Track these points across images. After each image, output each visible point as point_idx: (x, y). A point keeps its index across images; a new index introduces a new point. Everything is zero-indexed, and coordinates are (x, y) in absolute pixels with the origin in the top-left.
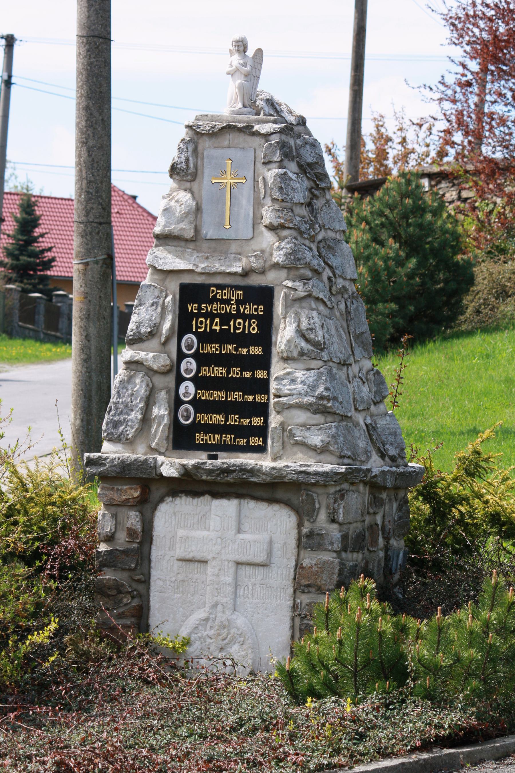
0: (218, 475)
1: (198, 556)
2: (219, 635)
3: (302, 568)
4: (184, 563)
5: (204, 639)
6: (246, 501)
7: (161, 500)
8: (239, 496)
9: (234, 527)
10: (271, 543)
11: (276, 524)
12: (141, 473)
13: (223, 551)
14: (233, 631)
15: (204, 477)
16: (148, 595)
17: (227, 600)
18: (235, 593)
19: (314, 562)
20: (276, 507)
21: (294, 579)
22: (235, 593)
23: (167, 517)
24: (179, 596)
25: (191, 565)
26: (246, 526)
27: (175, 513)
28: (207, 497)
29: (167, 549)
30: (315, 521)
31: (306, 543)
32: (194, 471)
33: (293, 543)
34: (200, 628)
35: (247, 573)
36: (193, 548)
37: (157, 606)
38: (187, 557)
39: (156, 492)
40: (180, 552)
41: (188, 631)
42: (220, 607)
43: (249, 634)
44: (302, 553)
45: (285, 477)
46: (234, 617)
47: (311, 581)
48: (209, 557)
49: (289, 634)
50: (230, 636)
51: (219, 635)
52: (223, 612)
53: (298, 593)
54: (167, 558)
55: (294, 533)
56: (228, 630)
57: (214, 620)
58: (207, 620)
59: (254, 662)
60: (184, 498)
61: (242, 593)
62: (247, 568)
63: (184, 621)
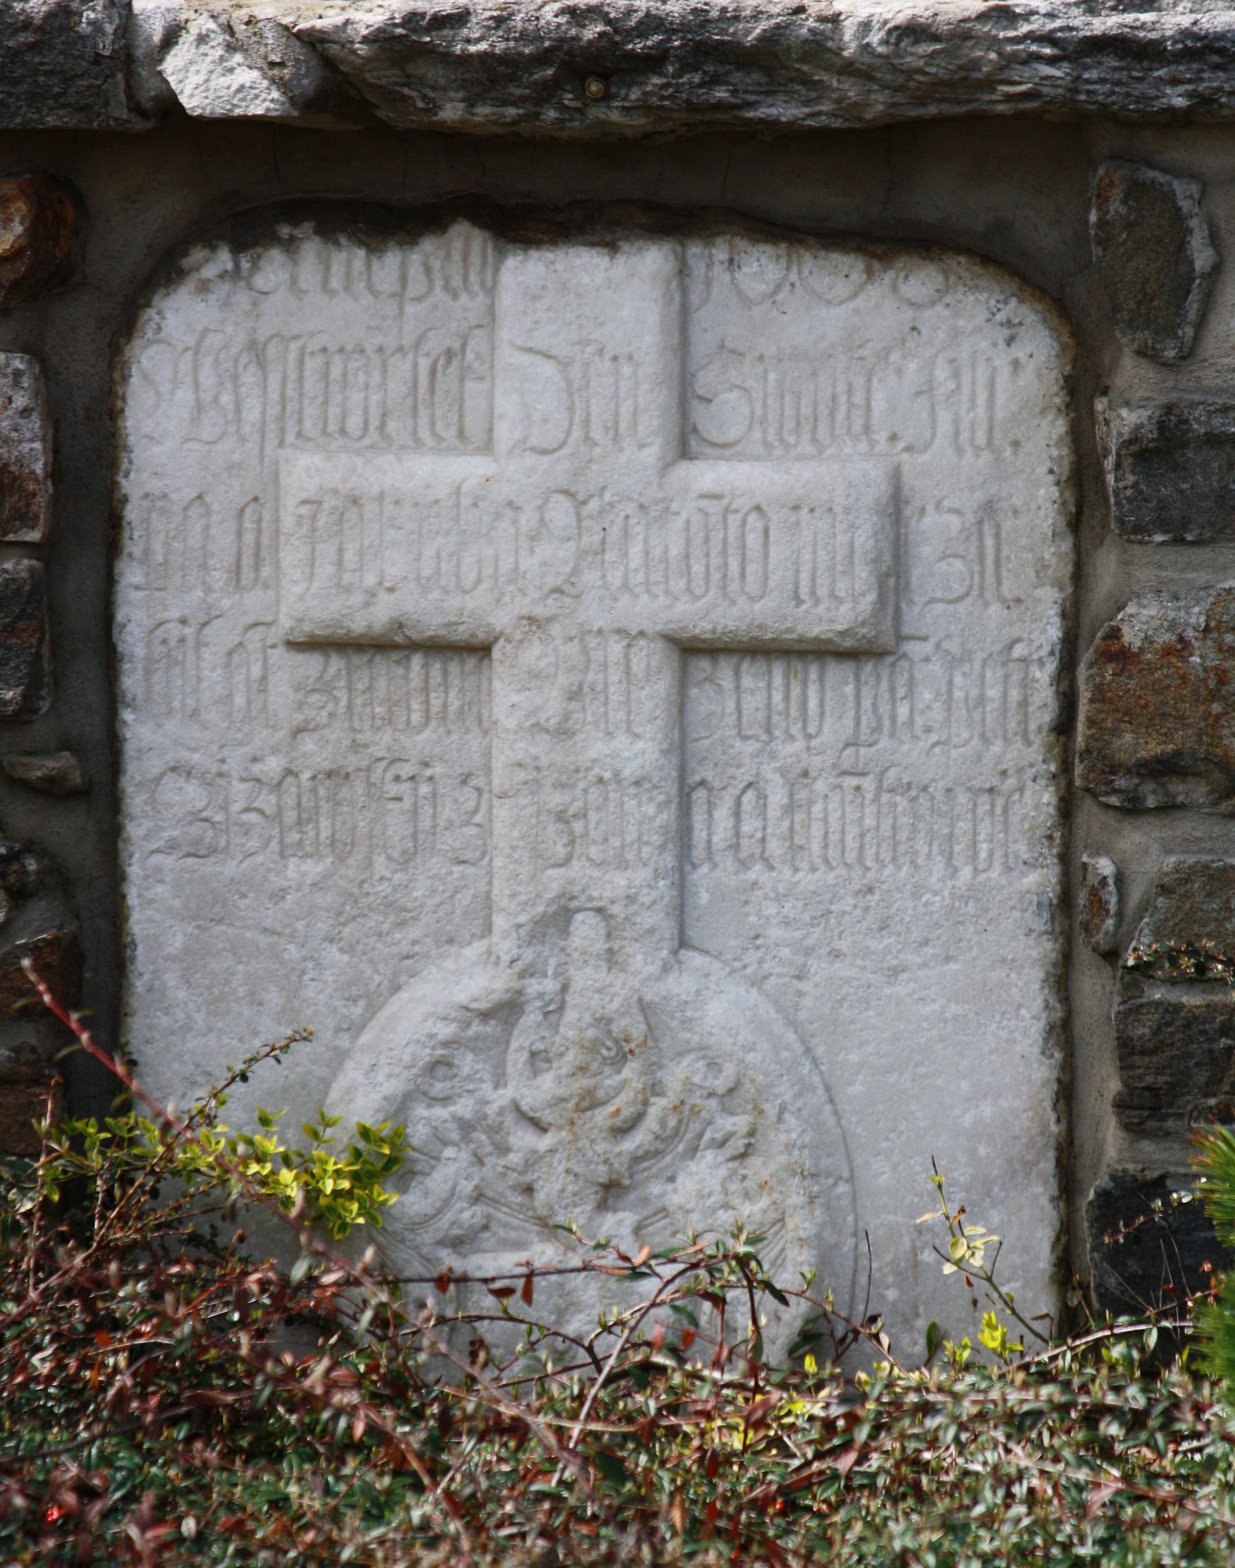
0: (547, 93)
1: (429, 612)
2: (589, 1102)
3: (1116, 654)
4: (336, 663)
5: (495, 1130)
6: (720, 252)
7: (164, 270)
8: (676, 220)
9: (651, 421)
10: (896, 508)
11: (927, 389)
12: (34, 97)
13: (590, 577)
14: (676, 1075)
15: (451, 112)
16: (115, 876)
17: (630, 880)
18: (682, 837)
19: (1197, 616)
20: (920, 281)
21: (1064, 726)
22: (682, 837)
23: (207, 377)
24: (314, 869)
25: (384, 676)
26: (728, 413)
27: (257, 351)
28: (466, 238)
29: (218, 577)
30: (1188, 354)
31: (1139, 497)
32: (387, 76)
33: (1037, 499)
34: (467, 1063)
35: (752, 704)
36: (395, 566)
37: (176, 941)
38: (358, 625)
39: (125, 224)
40: (305, 593)
41: (392, 1087)
42: (585, 930)
43: (785, 1091)
44: (1107, 567)
45: (989, 84)
46: (680, 985)
47: (1181, 740)
48: (501, 619)
49: (1036, 1072)
50: (658, 1105)
51: (589, 1102)
52: (611, 958)
53: (1090, 816)
54: (221, 635)
55: (1047, 436)
56: (651, 1068)
57: (554, 1011)
58: (506, 1011)
59: (826, 1259)
60: (311, 249)
61: (721, 836)
62: (751, 676)
63: (356, 1029)
